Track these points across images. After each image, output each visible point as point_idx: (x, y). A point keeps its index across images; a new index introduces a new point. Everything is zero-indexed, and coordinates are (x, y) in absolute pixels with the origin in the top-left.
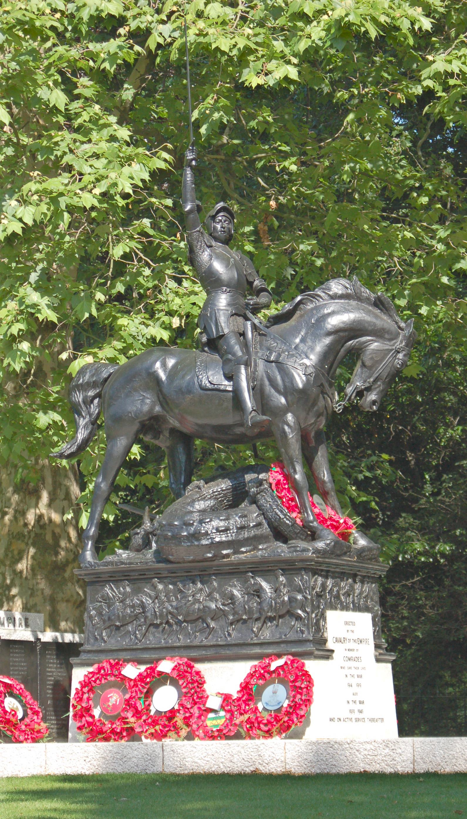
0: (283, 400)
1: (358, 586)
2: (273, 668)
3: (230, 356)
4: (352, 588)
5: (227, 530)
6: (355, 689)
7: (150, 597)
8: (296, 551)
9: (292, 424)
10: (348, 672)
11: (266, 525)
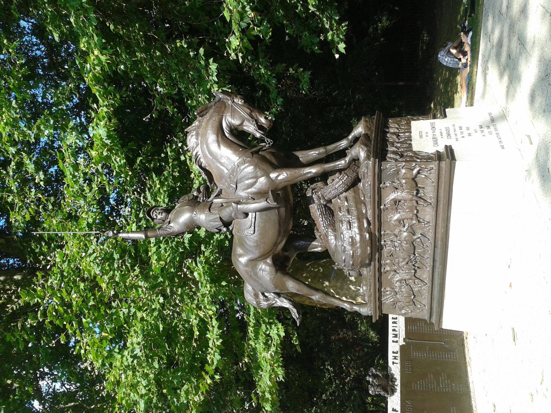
1: (392, 130)
3: (233, 215)
4: (394, 133)
5: (349, 223)
6: (471, 131)
7: (394, 275)
8: (367, 173)
9: (277, 174)
10: (459, 136)
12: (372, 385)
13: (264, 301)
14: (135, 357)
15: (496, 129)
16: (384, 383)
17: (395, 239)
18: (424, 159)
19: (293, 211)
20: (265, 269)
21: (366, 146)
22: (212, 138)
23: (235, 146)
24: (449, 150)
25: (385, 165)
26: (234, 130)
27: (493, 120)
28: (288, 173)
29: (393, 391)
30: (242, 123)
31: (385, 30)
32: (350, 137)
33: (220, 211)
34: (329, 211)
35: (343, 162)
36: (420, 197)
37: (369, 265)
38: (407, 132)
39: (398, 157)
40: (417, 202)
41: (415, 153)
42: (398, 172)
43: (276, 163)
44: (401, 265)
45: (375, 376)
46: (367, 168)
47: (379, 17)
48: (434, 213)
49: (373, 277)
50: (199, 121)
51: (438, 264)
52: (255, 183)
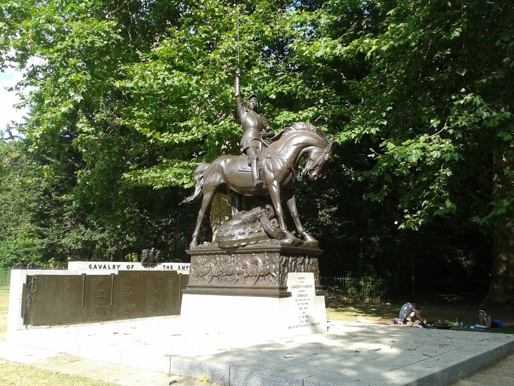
0: (272, 175)
1: (307, 260)
2: (177, 163)
5: (244, 233)
9: (276, 185)
11: (263, 231)
12: (149, 251)
13: (199, 178)
14: (164, 80)
15: (305, 326)
16: (151, 259)
17: (235, 263)
18: (282, 280)
19: (253, 197)
20: (217, 179)
21: (292, 243)
22: (301, 139)
23: (296, 156)
24: (289, 295)
25: (277, 256)
26: (306, 155)
27: (313, 325)
28: (277, 193)
29: (145, 266)
30: (311, 160)
31: (459, 264)
32: (304, 233)
33: (254, 147)
34: (255, 220)
35: (284, 229)
36: (259, 278)
37: (219, 247)
38: (304, 270)
39: (283, 263)
40: (256, 276)
41: (287, 273)
42: (274, 263)
43: (284, 184)
44: (220, 267)
45: (155, 253)
46: (276, 244)
47: (471, 257)
48: (250, 286)
49: (212, 249)
50: (313, 130)
51: (220, 290)
52: (270, 171)
